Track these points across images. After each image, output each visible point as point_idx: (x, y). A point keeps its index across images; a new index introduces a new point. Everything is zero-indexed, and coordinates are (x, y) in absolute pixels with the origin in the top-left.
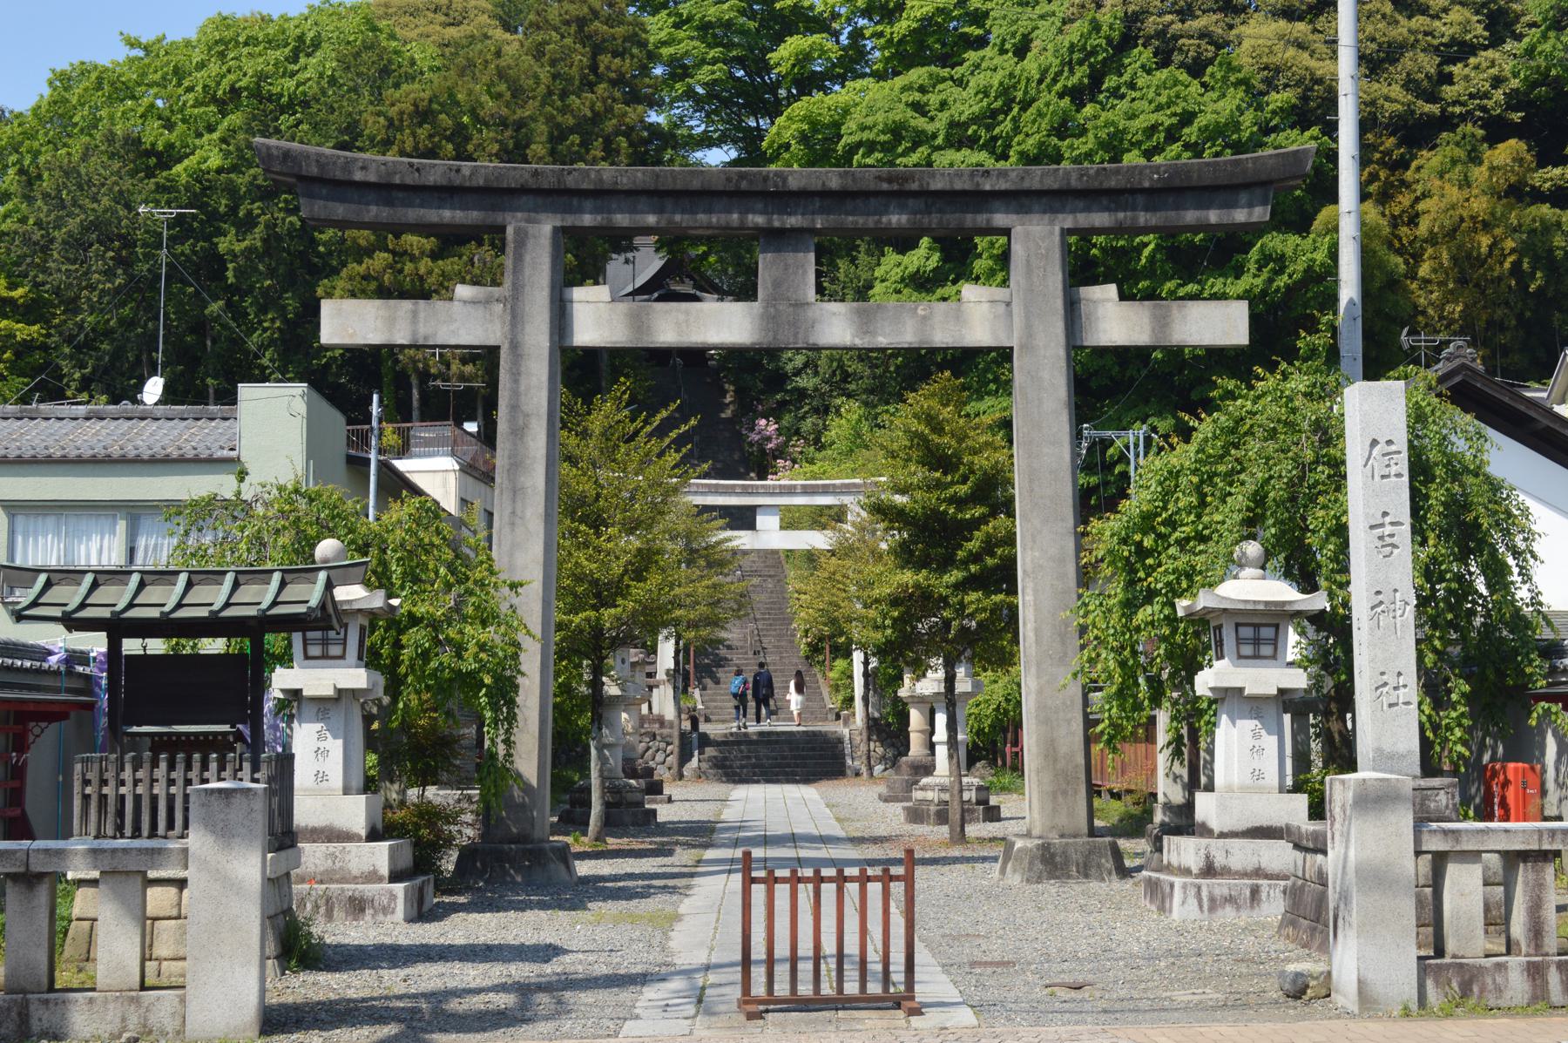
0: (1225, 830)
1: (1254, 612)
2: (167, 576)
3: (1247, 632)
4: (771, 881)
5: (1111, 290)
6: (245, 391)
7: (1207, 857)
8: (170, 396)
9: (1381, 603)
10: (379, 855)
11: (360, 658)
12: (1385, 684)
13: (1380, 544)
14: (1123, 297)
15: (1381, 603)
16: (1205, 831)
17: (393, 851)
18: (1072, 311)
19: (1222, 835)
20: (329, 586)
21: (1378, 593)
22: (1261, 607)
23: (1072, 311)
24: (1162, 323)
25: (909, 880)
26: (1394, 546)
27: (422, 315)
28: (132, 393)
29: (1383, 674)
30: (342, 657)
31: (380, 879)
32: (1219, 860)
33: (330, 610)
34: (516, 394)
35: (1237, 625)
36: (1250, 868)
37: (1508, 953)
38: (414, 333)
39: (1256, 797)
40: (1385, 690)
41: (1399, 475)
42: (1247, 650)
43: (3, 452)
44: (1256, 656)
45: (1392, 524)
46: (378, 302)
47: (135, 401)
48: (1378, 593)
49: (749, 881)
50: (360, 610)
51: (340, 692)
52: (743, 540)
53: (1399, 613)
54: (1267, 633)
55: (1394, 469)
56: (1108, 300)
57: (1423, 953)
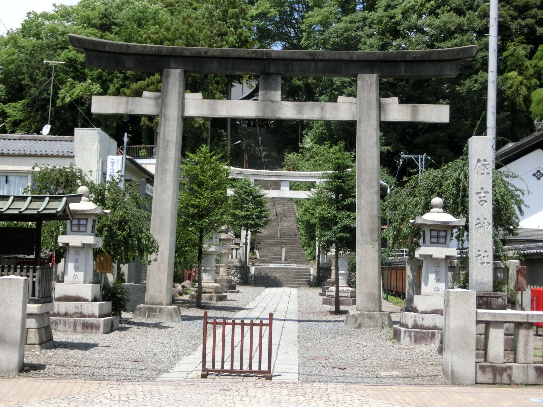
0: (423, 310)
1: (437, 226)
2: (24, 198)
3: (434, 233)
4: (215, 324)
5: (396, 99)
6: (77, 131)
7: (415, 320)
8: (52, 132)
9: (479, 223)
10: (95, 308)
11: (93, 232)
12: (480, 255)
13: (479, 200)
14: (400, 103)
15: (479, 223)
16: (415, 310)
17: (100, 307)
18: (380, 107)
19: (422, 312)
20: (67, 204)
21: (478, 219)
22: (439, 224)
23: (380, 107)
24: (415, 113)
25: (270, 325)
26: (486, 201)
27: (130, 102)
28: (38, 131)
29: (479, 251)
30: (85, 231)
31: (96, 317)
32: (420, 322)
33: (68, 212)
34: (164, 134)
35: (431, 230)
36: (431, 326)
37: (515, 362)
38: (127, 109)
39: (435, 298)
40: (479, 257)
41: (488, 173)
42: (434, 240)
43: (1, 152)
44: (438, 243)
45: (485, 192)
46: (114, 97)
47: (39, 133)
48: (478, 219)
49: (206, 323)
50: (92, 214)
51: (84, 244)
52: (271, 193)
53: (486, 227)
54: (442, 234)
55: (486, 171)
56: (395, 103)
57: (478, 360)
